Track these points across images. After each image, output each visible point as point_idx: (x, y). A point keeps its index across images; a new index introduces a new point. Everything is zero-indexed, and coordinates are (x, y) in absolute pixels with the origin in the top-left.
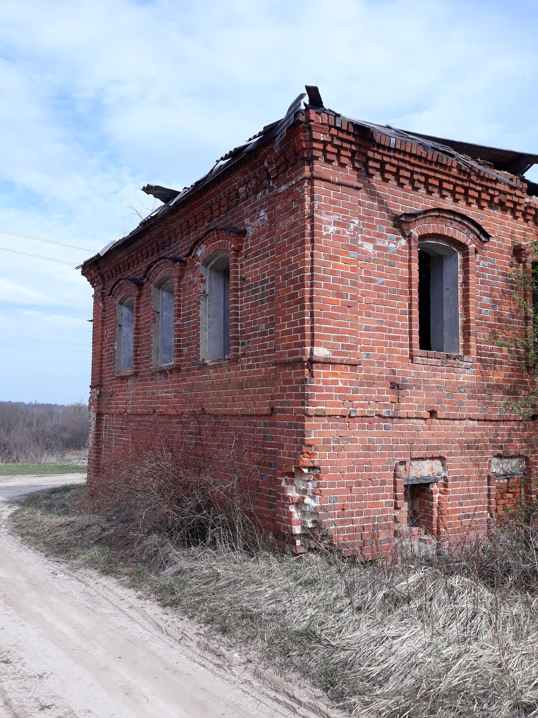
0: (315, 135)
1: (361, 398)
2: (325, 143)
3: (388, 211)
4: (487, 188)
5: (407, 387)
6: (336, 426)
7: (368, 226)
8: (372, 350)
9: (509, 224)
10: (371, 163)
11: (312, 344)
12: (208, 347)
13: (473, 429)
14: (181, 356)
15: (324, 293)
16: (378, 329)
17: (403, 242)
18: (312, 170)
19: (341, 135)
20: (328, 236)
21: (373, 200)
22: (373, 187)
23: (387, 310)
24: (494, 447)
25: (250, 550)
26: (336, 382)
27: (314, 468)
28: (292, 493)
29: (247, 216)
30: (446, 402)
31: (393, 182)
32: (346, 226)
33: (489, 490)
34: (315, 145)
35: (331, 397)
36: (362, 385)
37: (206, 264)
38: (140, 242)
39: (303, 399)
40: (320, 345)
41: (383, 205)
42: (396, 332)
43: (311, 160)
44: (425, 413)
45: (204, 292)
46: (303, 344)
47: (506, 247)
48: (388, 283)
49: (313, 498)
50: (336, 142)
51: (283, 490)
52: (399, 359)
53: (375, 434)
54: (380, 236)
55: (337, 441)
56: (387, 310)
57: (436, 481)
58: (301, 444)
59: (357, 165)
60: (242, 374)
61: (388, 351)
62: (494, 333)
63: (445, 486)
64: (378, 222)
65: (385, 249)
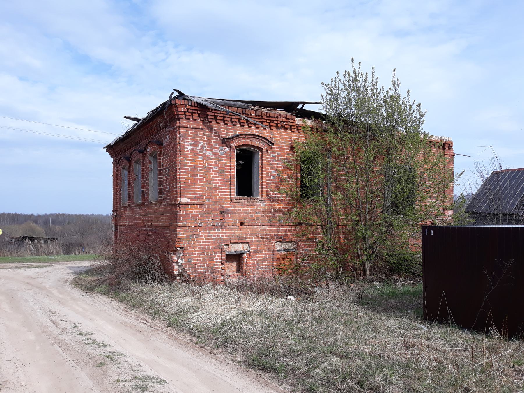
0: (179, 109)
1: (204, 218)
2: (185, 112)
3: (219, 137)
4: (273, 121)
5: (228, 213)
6: (192, 231)
7: (209, 144)
8: (211, 198)
9: (288, 135)
10: (209, 117)
11: (180, 197)
12: (153, 195)
13: (265, 230)
14: (144, 198)
15: (185, 175)
16: (214, 189)
17: (228, 150)
18: (180, 123)
19: (191, 108)
20: (188, 151)
21: (211, 133)
22: (212, 127)
23: (219, 180)
24: (277, 238)
25: (161, 282)
26: (192, 212)
27: (182, 248)
28: (175, 258)
29: (163, 137)
30: (249, 219)
31: (222, 123)
32: (197, 146)
33: (273, 256)
34: (180, 113)
35: (189, 218)
36: (205, 213)
37: (151, 155)
38: (128, 140)
39: (176, 220)
40: (184, 197)
41: (217, 134)
42: (223, 189)
43: (179, 119)
44: (238, 223)
45: (151, 168)
46: (177, 197)
47: (286, 146)
48: (219, 168)
49: (182, 260)
50: (190, 111)
51: (172, 257)
52: (225, 201)
53: (212, 233)
54: (215, 148)
55: (193, 236)
56: (219, 180)
57: (245, 252)
58: (177, 239)
59: (201, 119)
60: (163, 208)
61: (219, 198)
62: (278, 186)
63: (250, 255)
64: (214, 142)
65: (218, 154)
